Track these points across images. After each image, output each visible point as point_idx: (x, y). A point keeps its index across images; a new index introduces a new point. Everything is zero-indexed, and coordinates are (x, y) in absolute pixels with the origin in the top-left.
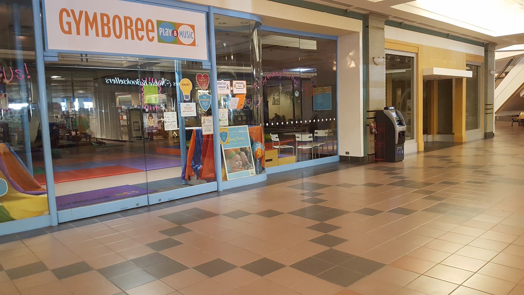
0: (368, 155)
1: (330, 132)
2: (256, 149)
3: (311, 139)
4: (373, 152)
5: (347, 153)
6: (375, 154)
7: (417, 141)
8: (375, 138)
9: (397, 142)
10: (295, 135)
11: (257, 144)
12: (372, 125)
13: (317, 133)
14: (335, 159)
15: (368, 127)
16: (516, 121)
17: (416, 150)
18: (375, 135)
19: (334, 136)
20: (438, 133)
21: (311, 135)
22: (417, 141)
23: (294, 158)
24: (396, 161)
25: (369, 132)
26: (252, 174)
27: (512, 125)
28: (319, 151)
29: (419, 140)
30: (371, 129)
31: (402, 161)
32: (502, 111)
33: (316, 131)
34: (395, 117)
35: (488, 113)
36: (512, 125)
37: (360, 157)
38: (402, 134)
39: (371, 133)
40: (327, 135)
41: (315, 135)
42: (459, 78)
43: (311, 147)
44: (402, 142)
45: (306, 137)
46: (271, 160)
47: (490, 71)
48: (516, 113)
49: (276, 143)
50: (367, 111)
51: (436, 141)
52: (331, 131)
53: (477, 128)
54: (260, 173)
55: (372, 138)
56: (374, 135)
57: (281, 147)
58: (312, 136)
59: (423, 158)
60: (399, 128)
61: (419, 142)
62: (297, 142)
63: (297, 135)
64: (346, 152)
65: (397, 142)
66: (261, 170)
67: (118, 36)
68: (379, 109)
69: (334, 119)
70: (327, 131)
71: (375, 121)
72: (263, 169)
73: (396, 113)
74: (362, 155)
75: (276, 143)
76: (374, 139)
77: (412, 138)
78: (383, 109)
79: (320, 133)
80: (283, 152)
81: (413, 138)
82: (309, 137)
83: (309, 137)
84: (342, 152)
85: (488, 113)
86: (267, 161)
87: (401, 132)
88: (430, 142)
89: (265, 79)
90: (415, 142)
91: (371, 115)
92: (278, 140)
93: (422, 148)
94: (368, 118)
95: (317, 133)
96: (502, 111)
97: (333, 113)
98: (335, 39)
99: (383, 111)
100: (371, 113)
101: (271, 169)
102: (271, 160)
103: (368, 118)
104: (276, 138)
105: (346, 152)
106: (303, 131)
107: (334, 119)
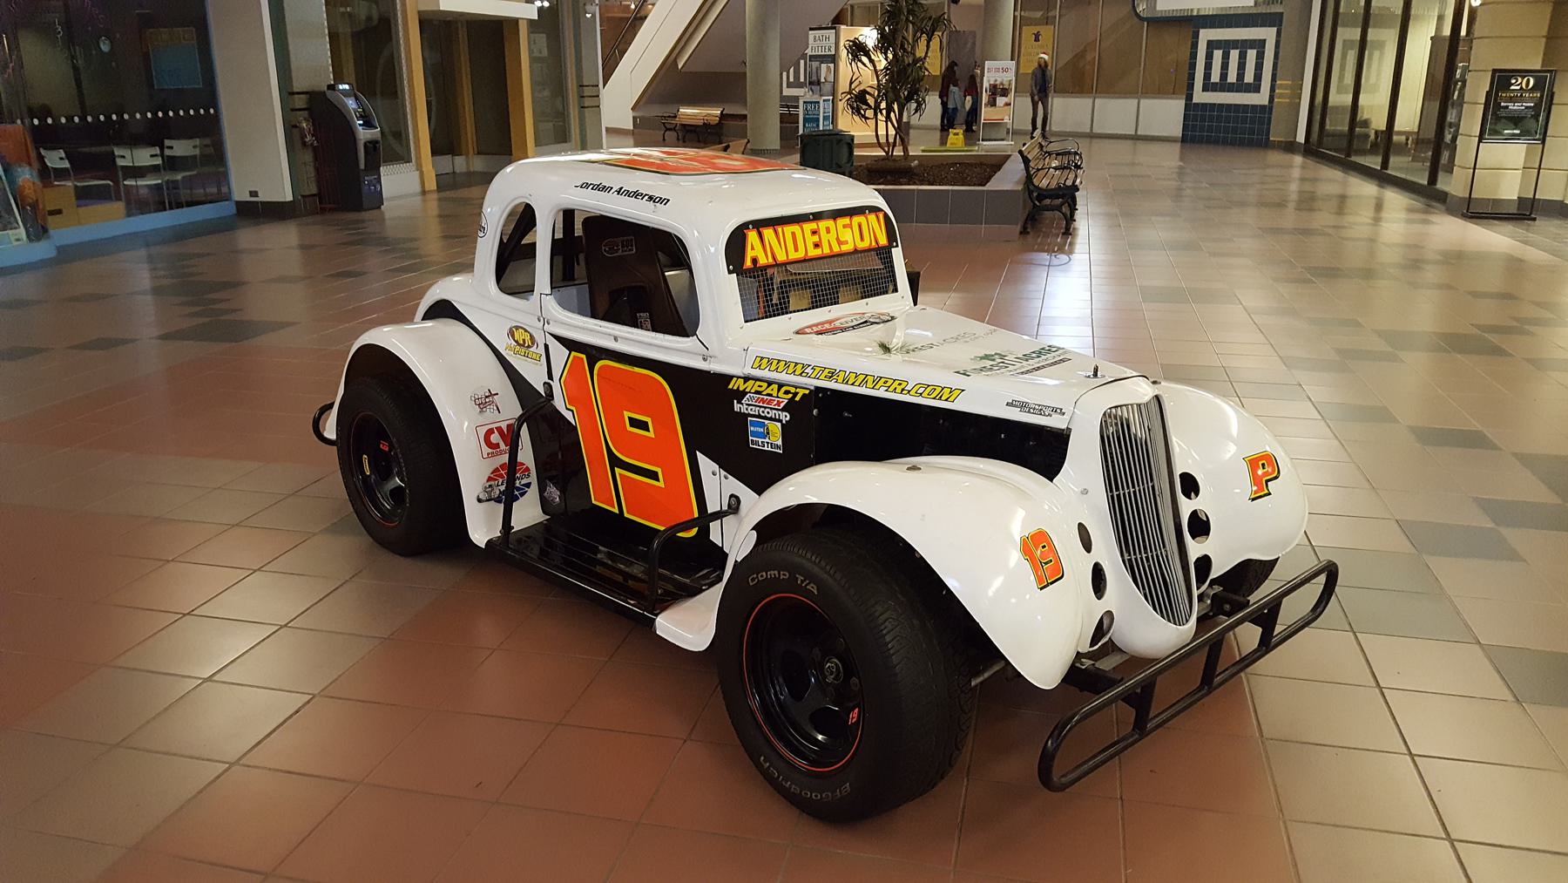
0: (303, 196)
1: (206, 146)
2: (20, 181)
3: (158, 161)
4: (314, 190)
5: (254, 194)
6: (319, 195)
7: (419, 168)
8: (316, 159)
9: (362, 166)
10: (113, 153)
11: (19, 170)
12: (304, 125)
13: (172, 148)
14: (225, 209)
15: (295, 131)
16: (670, 129)
17: (418, 189)
18: (315, 149)
19: (215, 157)
20: (478, 153)
21: (157, 150)
22: (419, 168)
23: (120, 206)
24: (365, 206)
25: (298, 144)
26: (18, 240)
27: (664, 139)
28: (183, 198)
29: (424, 165)
30: (303, 137)
31: (380, 207)
32: (646, 103)
33: (167, 142)
34: (354, 109)
35: (588, 107)
36: (664, 139)
37: (285, 202)
38: (372, 146)
39: (304, 144)
40: (197, 152)
41: (167, 152)
42: (486, 19)
43: (160, 181)
44: (374, 167)
45: (144, 157)
46: (59, 212)
47: (585, 4)
48: (669, 110)
49: (61, 174)
50: (287, 92)
51: (476, 170)
52: (207, 141)
53: (566, 142)
54: (38, 239)
55: (308, 157)
56: (310, 149)
57: (79, 184)
58: (159, 152)
59: (435, 204)
60: (363, 134)
61: (424, 169)
62: (119, 169)
63: (118, 151)
64: (251, 192)
65: (362, 166)
66: (38, 231)
67: (105, 53)
68: (317, 89)
69: (212, 111)
70: (197, 141)
71: (311, 115)
72: (45, 230)
73: (357, 99)
74: (290, 198)
75: (61, 174)
76: (311, 160)
77: (405, 159)
78: (326, 88)
79: (181, 148)
80: (84, 195)
81: (409, 161)
82: (152, 156)
83: (152, 156)
84: (240, 194)
85: (588, 107)
86: (52, 213)
87: (369, 142)
88: (460, 173)
89: (13, 5)
90: (414, 168)
91: (300, 102)
92: (66, 164)
93: (432, 184)
94: (293, 110)
95: (172, 148)
96: (646, 103)
97: (209, 96)
98: (82, 202)
99: (324, 92)
100: (300, 99)
101: (65, 233)
102: (59, 212)
103: (293, 110)
104: (61, 159)
105: (251, 192)
106: (135, 141)
107: (212, 111)
